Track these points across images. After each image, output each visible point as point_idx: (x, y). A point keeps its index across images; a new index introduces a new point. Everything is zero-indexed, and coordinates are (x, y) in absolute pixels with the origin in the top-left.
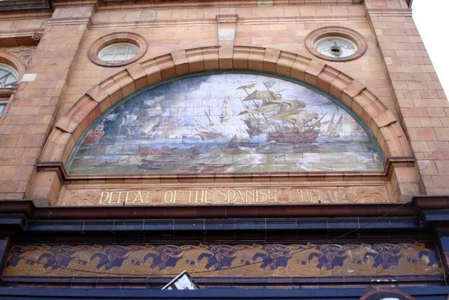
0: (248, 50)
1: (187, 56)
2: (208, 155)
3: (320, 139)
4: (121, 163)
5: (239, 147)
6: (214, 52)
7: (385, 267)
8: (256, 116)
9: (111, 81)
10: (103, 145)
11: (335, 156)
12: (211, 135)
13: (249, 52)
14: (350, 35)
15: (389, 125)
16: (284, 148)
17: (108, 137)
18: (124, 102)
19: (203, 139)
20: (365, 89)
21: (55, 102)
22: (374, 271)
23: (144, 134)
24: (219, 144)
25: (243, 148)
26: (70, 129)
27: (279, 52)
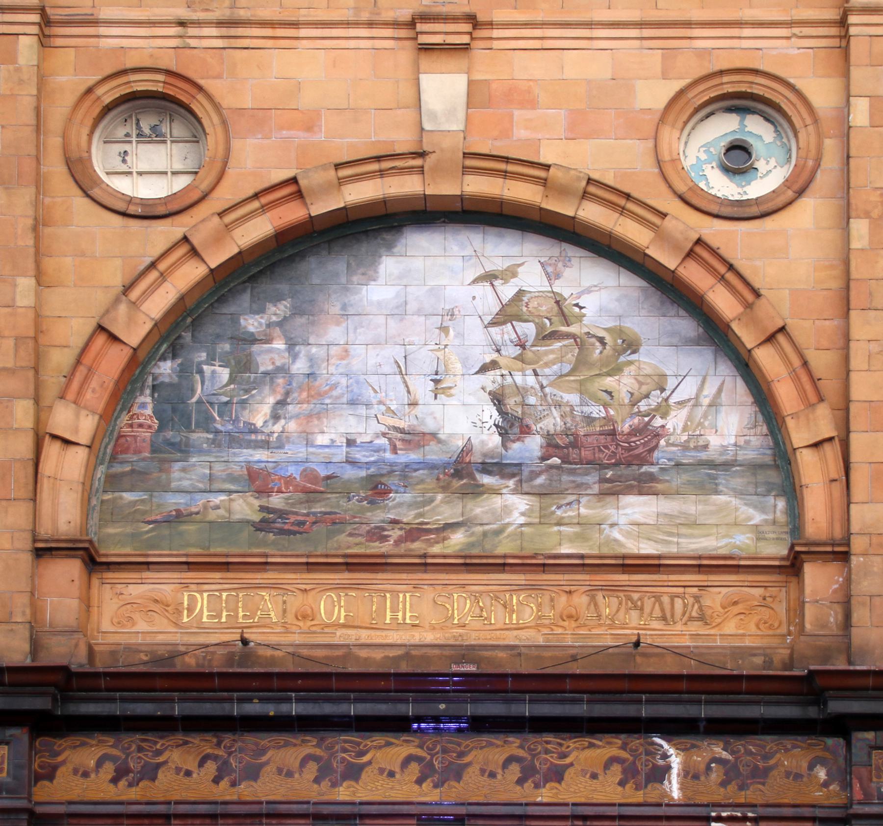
0: (502, 166)
1: (342, 182)
2: (407, 497)
3: (664, 454)
4: (212, 516)
5: (478, 476)
6: (410, 170)
7: (741, 788)
8: (519, 379)
9: (153, 275)
10: (163, 461)
11: (690, 506)
12: (414, 438)
13: (505, 174)
14: (783, 106)
15: (816, 445)
16: (579, 479)
17: (169, 434)
18: (189, 320)
19: (394, 450)
20: (782, 329)
22: (719, 795)
23: (255, 431)
24: (432, 467)
25: (487, 480)
26: (84, 437)
27: (584, 183)
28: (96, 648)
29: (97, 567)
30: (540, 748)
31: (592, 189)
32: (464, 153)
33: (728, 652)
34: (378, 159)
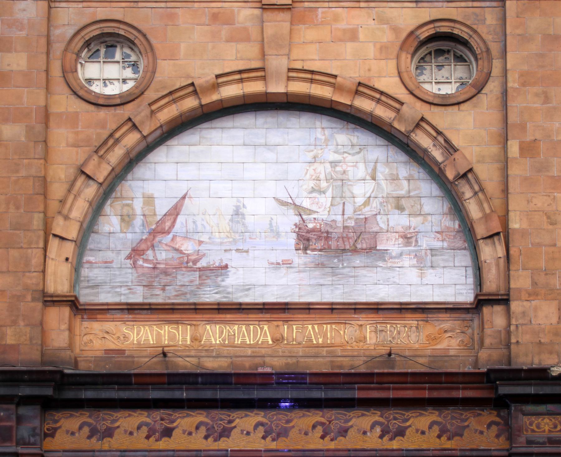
15: (491, 237)
20: (471, 170)
28: (78, 359)
29: (80, 311)
30: (333, 417)
31: (361, 88)
32: (289, 69)
33: (93, 359)
34: (240, 72)
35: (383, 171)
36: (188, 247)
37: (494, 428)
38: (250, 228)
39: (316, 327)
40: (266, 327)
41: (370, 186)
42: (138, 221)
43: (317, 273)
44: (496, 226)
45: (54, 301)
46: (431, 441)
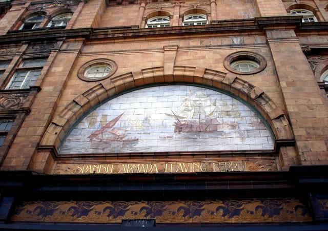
21: (52, 106)
34: (152, 68)
35: (219, 103)
36: (120, 133)
37: (300, 209)
38: (152, 125)
39: (184, 164)
40: (155, 165)
41: (213, 108)
42: (97, 124)
43: (185, 141)
44: (280, 112)
45: (43, 149)
46: (258, 218)
